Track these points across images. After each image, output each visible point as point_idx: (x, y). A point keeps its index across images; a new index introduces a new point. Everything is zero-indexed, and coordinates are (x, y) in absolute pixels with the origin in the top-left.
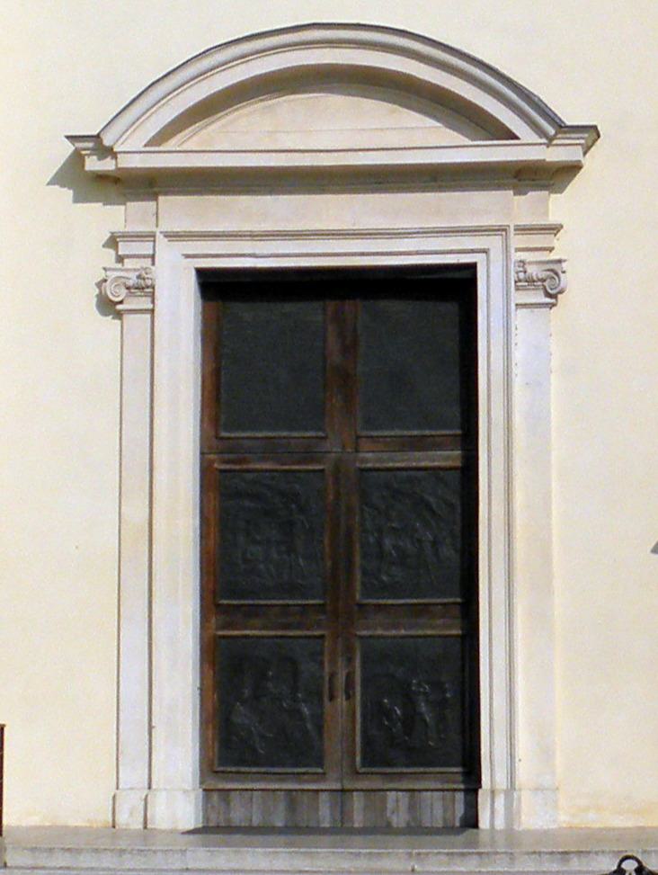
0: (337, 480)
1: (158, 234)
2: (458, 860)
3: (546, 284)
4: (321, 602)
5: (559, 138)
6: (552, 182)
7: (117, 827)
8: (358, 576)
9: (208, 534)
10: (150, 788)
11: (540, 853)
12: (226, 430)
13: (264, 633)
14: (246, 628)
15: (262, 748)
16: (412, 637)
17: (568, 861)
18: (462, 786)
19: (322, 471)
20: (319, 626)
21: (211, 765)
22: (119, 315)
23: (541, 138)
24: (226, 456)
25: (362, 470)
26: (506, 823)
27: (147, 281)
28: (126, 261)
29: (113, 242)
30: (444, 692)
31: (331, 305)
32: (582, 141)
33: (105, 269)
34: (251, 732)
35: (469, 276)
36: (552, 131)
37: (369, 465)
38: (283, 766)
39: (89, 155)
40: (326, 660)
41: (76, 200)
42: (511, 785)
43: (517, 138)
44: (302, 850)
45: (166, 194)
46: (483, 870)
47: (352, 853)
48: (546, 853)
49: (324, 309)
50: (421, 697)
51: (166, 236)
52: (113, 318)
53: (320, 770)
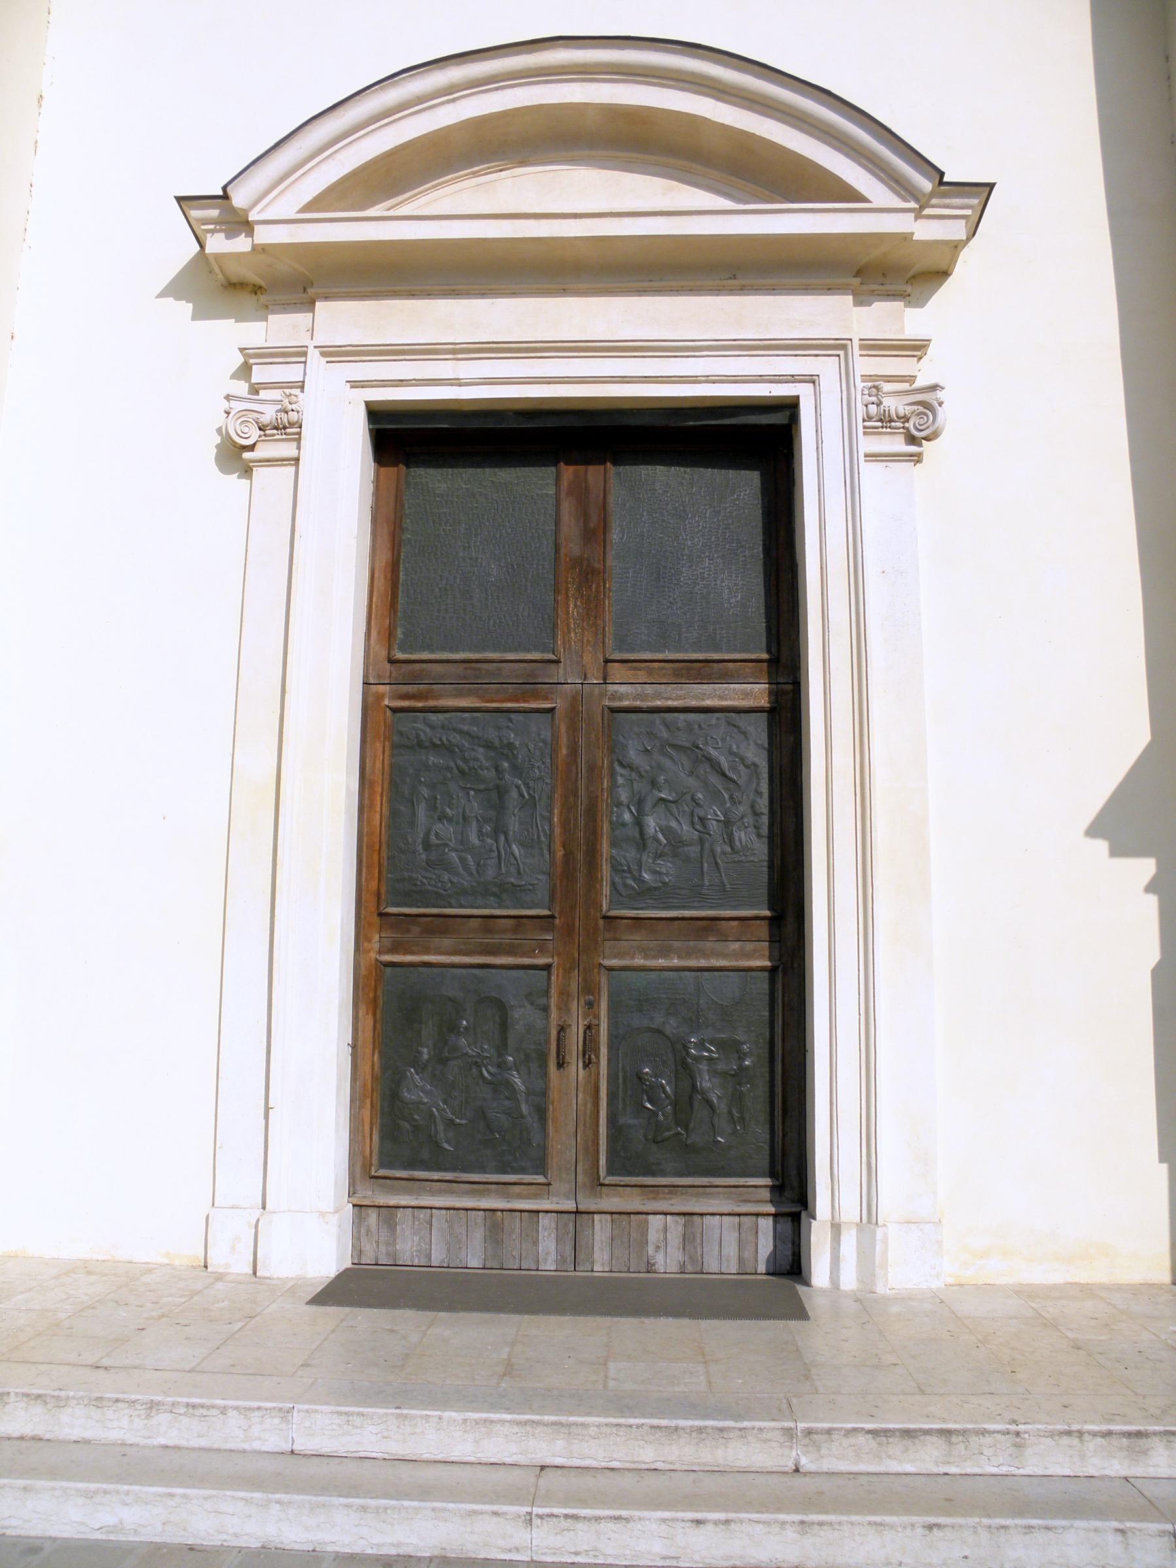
0: (573, 728)
1: (311, 348)
2: (896, 1446)
3: (910, 425)
4: (546, 912)
5: (933, 206)
6: (909, 289)
7: (209, 1270)
8: (606, 871)
9: (372, 806)
10: (264, 1208)
11: (1080, 1434)
12: (402, 649)
13: (456, 959)
14: (427, 951)
15: (448, 1142)
16: (690, 969)
17: (1145, 1452)
18: (771, 1209)
19: (552, 710)
20: (543, 951)
21: (367, 1167)
22: (247, 471)
23: (905, 200)
24: (405, 689)
25: (613, 710)
26: (860, 1281)
27: (290, 413)
28: (261, 392)
29: (245, 371)
30: (741, 1059)
31: (568, 472)
32: (968, 212)
33: (228, 398)
34: (432, 1115)
35: (786, 422)
36: (926, 185)
37: (626, 703)
38: (482, 1169)
39: (212, 232)
40: (553, 1001)
41: (196, 316)
42: (870, 1217)
43: (870, 202)
44: (546, 1418)
45: (326, 298)
46: (953, 1470)
47: (658, 1427)
48: (1095, 1434)
49: (558, 479)
50: (704, 1067)
51: (323, 354)
52: (239, 477)
53: (540, 1179)
